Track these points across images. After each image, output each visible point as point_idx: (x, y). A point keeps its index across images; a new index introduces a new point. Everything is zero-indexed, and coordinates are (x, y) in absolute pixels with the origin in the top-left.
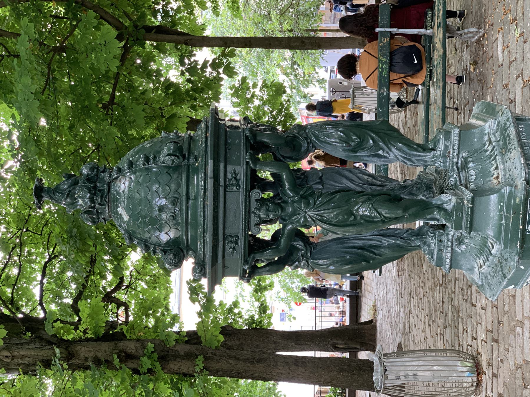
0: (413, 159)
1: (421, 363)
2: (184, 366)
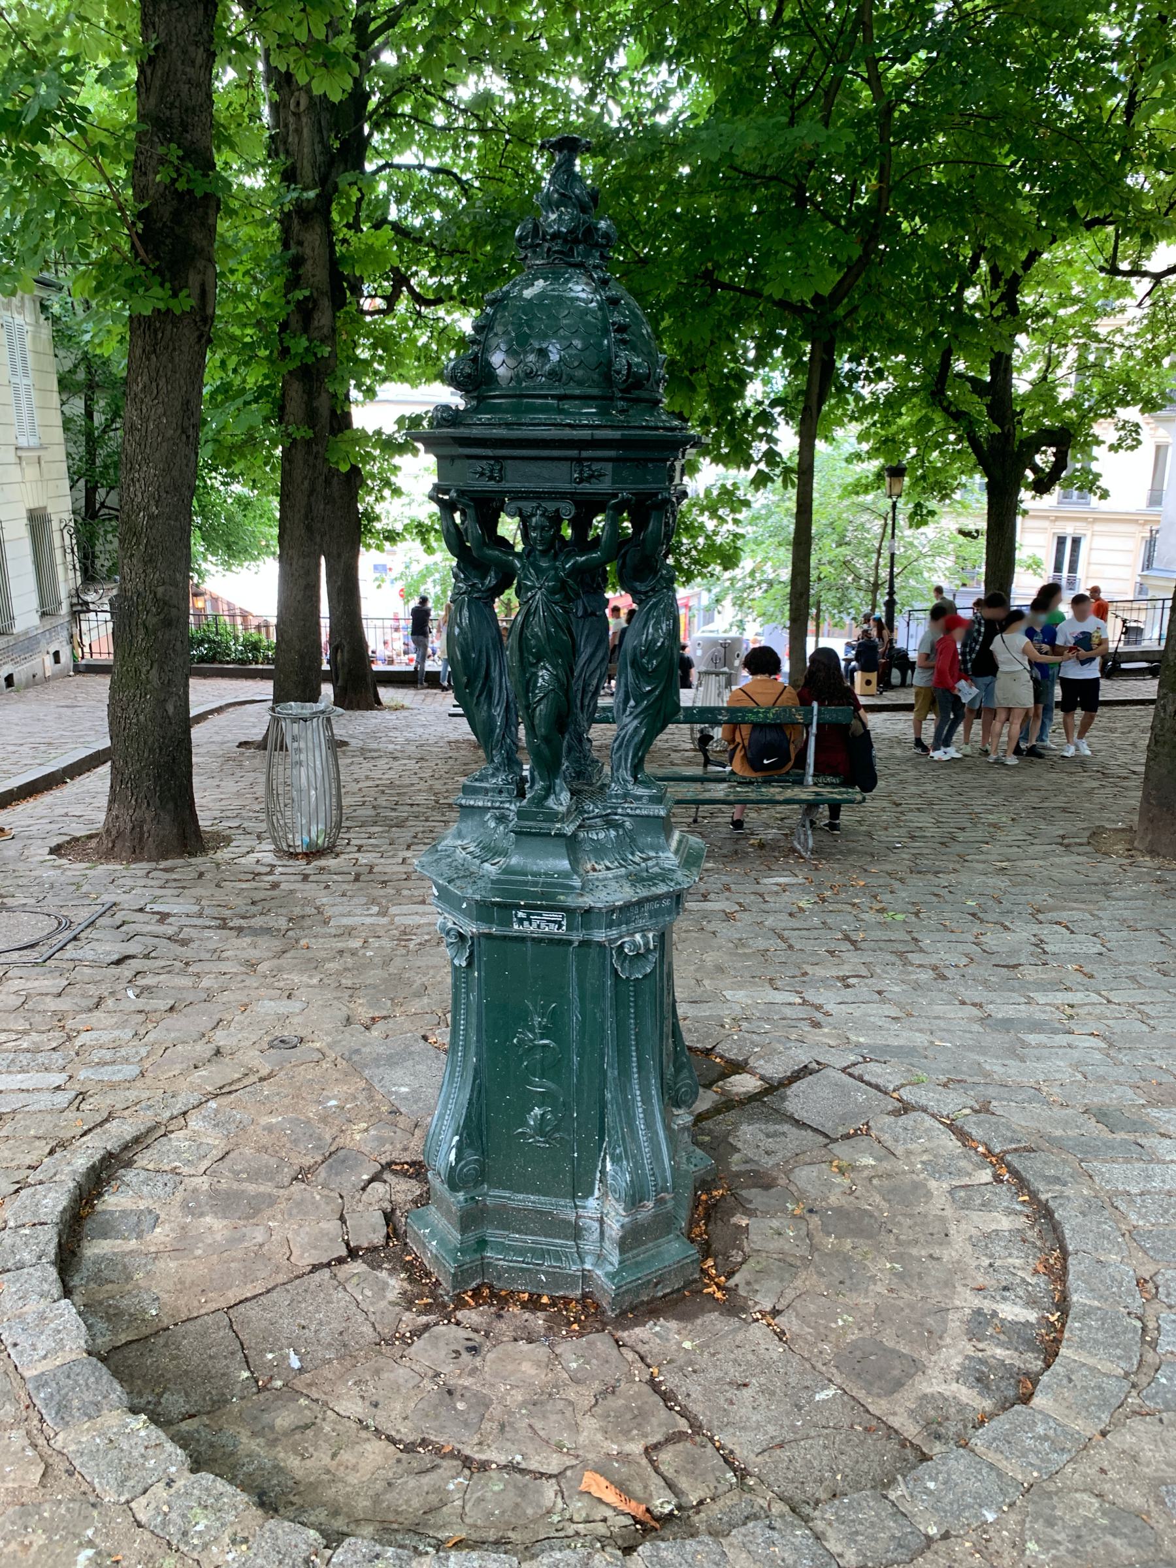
0: (622, 752)
1: (319, 773)
2: (295, 407)
